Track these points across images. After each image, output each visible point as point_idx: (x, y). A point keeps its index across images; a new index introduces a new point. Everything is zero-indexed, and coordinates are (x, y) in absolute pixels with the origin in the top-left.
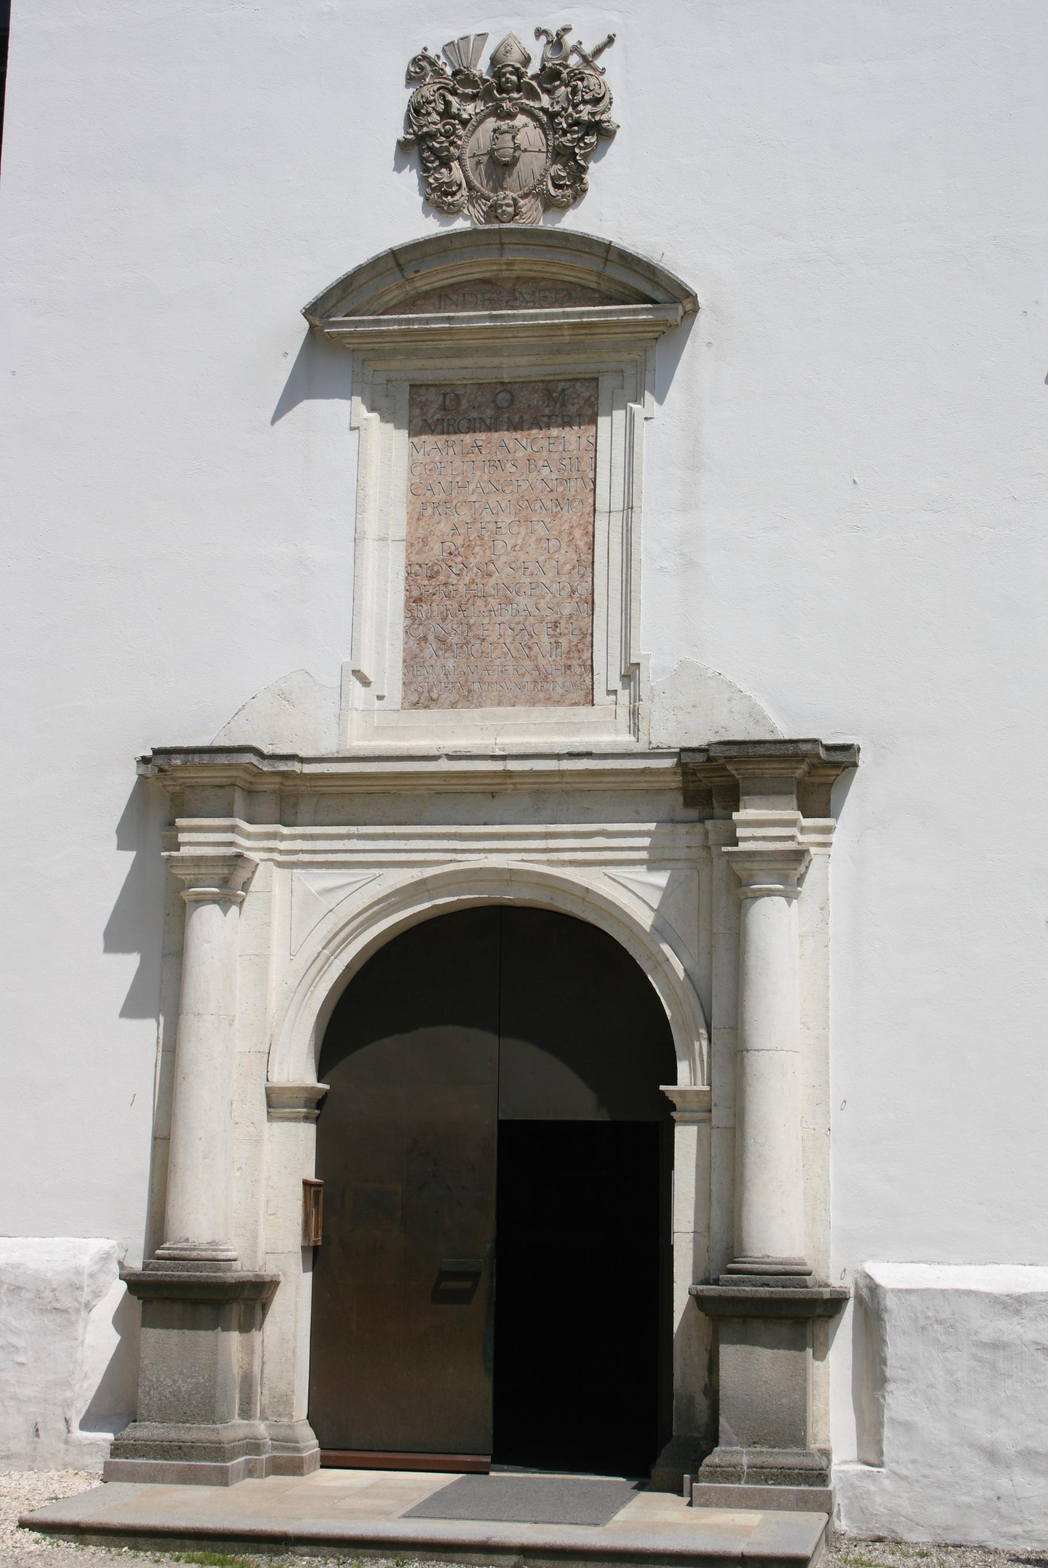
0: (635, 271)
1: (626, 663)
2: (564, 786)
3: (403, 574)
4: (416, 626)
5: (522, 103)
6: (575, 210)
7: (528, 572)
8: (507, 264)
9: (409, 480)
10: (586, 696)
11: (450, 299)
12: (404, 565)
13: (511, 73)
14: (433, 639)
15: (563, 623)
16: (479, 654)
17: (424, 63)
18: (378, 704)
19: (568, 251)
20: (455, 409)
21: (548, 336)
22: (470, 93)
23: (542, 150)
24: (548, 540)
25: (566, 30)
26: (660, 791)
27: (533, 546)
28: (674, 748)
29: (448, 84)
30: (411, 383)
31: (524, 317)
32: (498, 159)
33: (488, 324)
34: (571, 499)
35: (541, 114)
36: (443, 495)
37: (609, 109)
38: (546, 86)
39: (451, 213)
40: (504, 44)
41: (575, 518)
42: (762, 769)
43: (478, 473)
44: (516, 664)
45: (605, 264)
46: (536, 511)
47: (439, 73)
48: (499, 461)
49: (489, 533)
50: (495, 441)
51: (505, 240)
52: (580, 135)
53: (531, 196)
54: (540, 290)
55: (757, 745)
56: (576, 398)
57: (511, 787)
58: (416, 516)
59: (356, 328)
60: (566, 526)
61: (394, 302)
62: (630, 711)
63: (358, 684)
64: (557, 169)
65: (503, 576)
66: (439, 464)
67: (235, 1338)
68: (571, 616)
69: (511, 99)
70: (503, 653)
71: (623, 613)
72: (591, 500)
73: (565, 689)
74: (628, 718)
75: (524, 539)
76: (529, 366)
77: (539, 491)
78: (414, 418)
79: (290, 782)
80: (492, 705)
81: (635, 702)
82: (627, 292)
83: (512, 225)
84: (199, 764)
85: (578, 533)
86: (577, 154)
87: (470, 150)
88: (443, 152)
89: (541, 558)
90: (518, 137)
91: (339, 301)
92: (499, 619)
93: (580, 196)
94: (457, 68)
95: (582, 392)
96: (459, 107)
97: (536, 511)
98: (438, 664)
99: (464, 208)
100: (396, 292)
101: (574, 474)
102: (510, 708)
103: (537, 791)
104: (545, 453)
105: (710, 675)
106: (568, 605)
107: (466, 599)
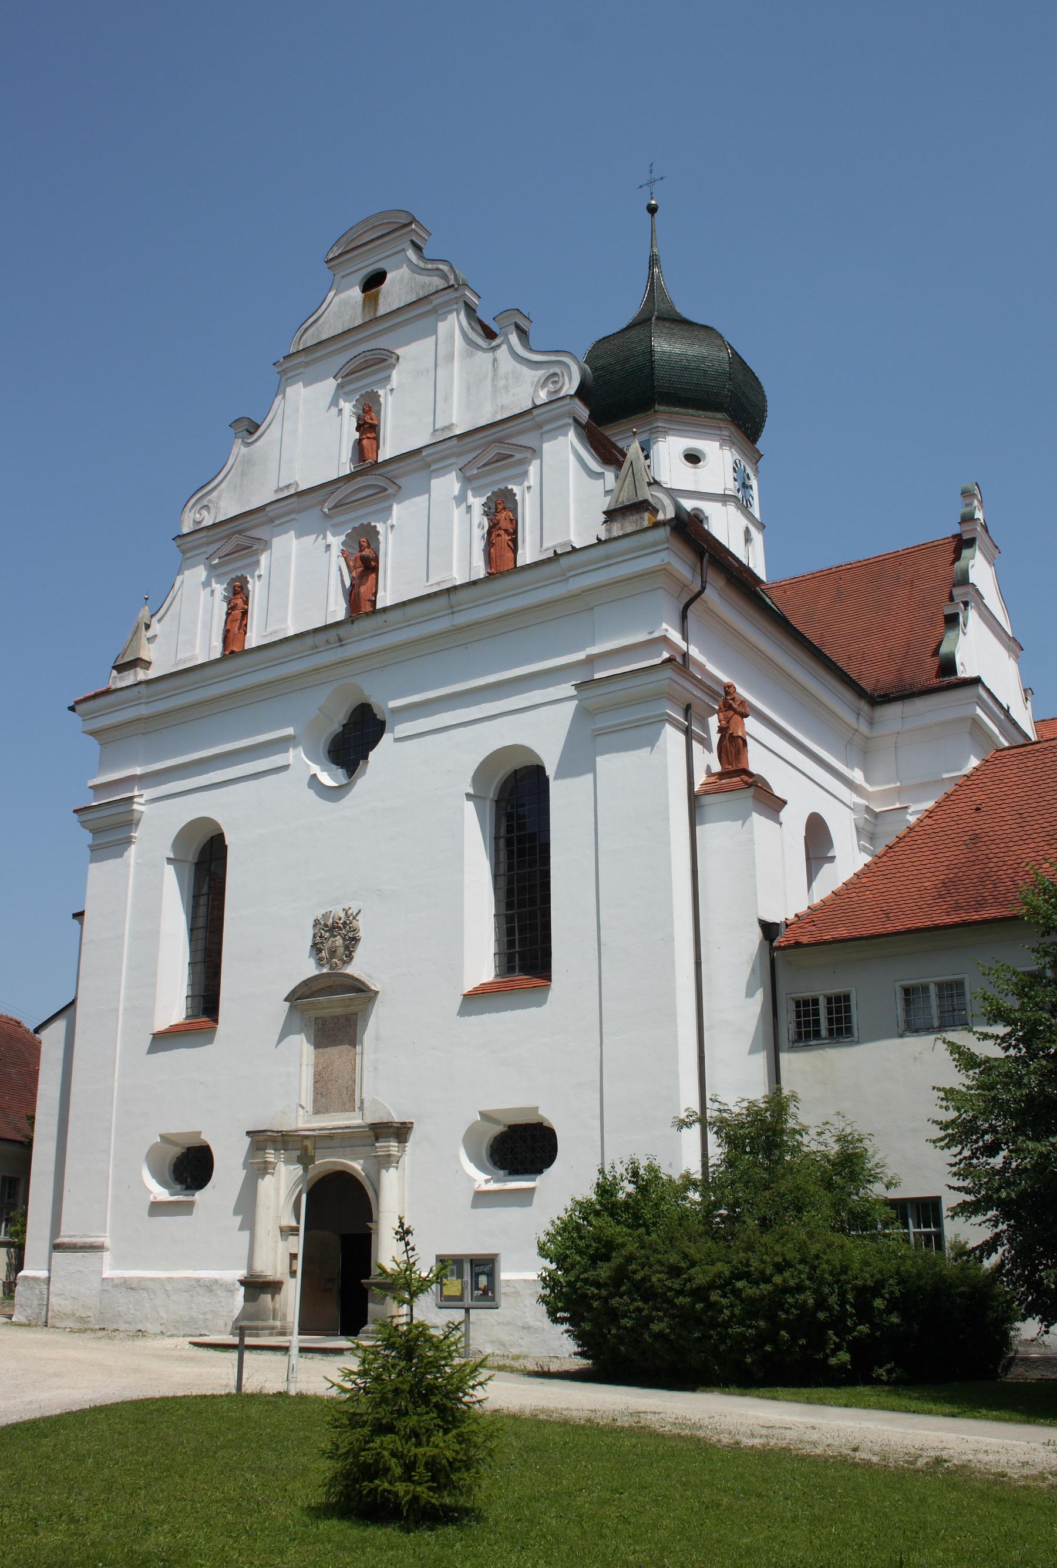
67: (269, 1296)
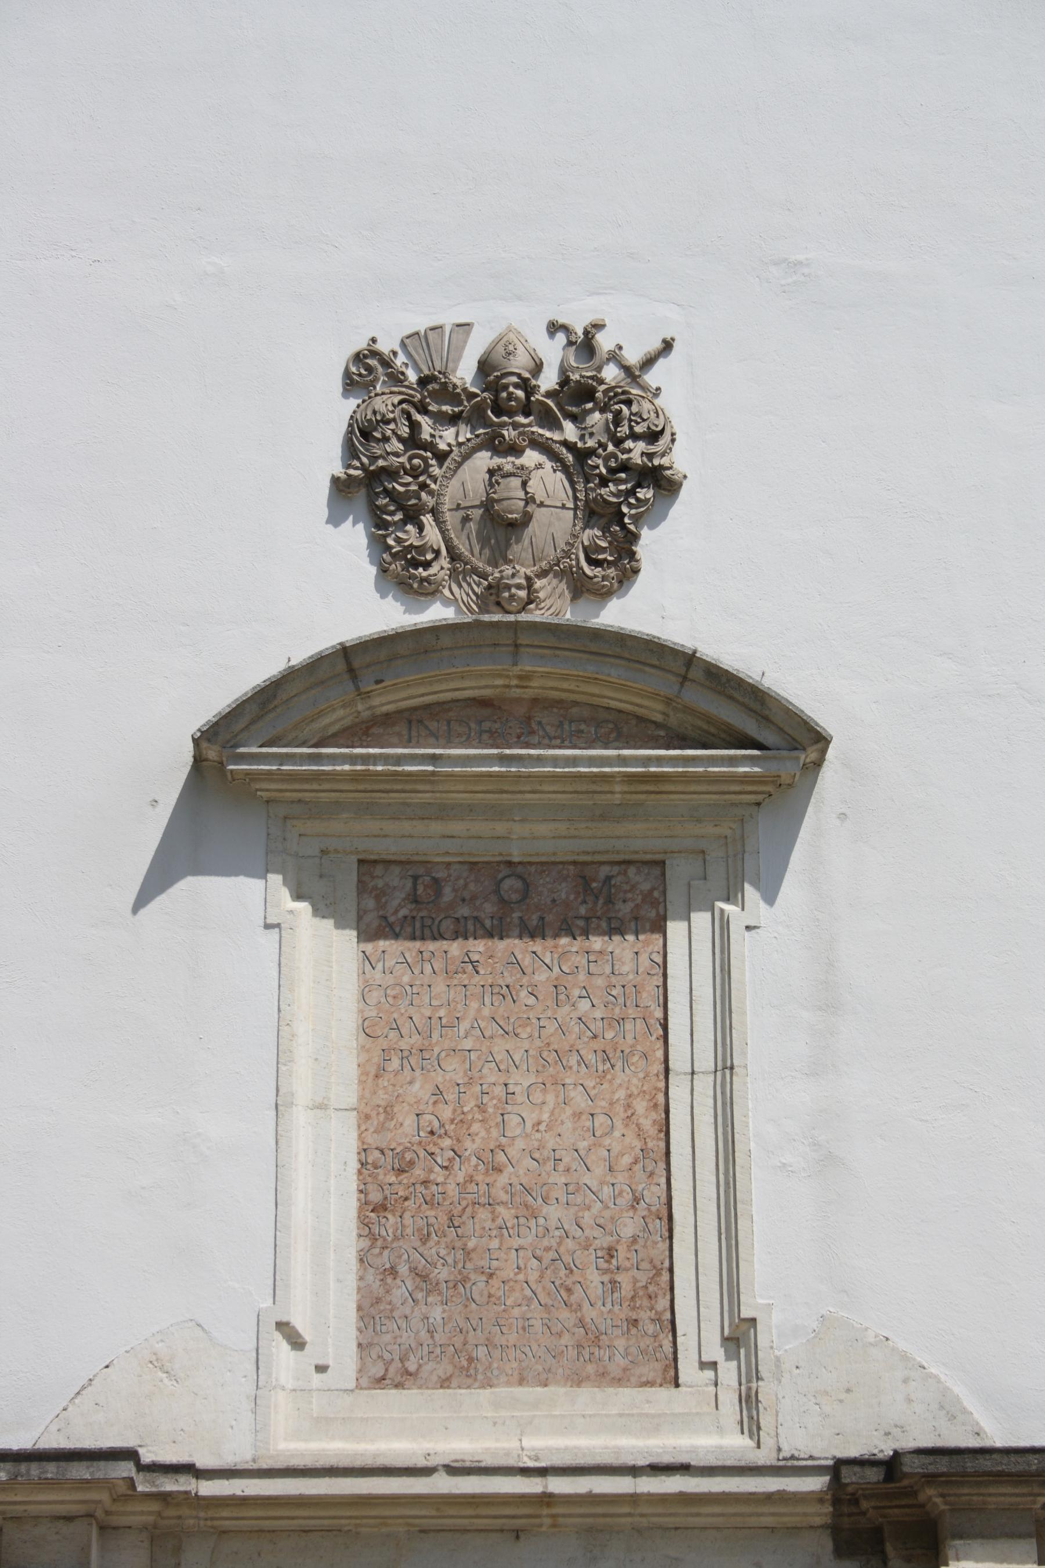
0: (731, 698)
1: (731, 1317)
2: (637, 1519)
3: (354, 1165)
4: (377, 1251)
5: (533, 433)
6: (622, 600)
7: (561, 1167)
8: (520, 677)
9: (361, 1011)
10: (665, 1370)
11: (426, 727)
12: (356, 1151)
13: (516, 386)
14: (407, 1273)
15: (622, 1250)
16: (485, 1299)
17: (373, 362)
18: (317, 1379)
19: (623, 662)
20: (433, 902)
21: (587, 792)
22: (450, 412)
23: (567, 506)
24: (592, 1115)
25: (599, 326)
26: (794, 1530)
27: (569, 1125)
28: (819, 1459)
29: (413, 396)
30: (361, 857)
31: (555, 761)
32: (499, 516)
33: (496, 769)
34: (627, 1051)
35: (564, 451)
36: (416, 1037)
37: (671, 449)
38: (570, 408)
39: (422, 594)
40: (502, 342)
41: (635, 1081)
42: (983, 1495)
43: (474, 1005)
44: (546, 1316)
45: (682, 684)
46: (571, 1068)
47: (397, 378)
48: (508, 987)
49: (495, 1102)
50: (500, 955)
51: (523, 640)
52: (629, 486)
53: (551, 575)
54: (571, 722)
55: (979, 1456)
56: (630, 891)
57: (548, 1521)
58: (373, 1071)
59: (281, 765)
60: (621, 1094)
61: (337, 727)
62: (740, 1395)
63: (285, 1346)
64: (591, 535)
65: (521, 1172)
66: (408, 988)
68: (635, 1239)
69: (516, 426)
70: (525, 1297)
71: (723, 1237)
72: (660, 1054)
73: (630, 1358)
74: (738, 1408)
75: (552, 1113)
76: (554, 837)
77: (574, 1036)
78: (365, 912)
79: (171, 1512)
80: (509, 1384)
81: (749, 1381)
82: (713, 730)
83: (523, 617)
84: (40, 1479)
85: (640, 1106)
86: (624, 515)
87: (451, 498)
88: (409, 500)
89: (582, 1145)
90: (530, 483)
91: (253, 722)
92: (516, 1242)
93: (628, 579)
94: (427, 372)
95: (638, 883)
96: (432, 431)
97: (571, 1068)
98: (417, 1313)
99: (444, 587)
100: (341, 713)
101: (630, 1011)
102: (539, 1389)
103: (590, 1530)
104: (582, 976)
105: (872, 1340)
106: (629, 1221)
107: (460, 1208)
